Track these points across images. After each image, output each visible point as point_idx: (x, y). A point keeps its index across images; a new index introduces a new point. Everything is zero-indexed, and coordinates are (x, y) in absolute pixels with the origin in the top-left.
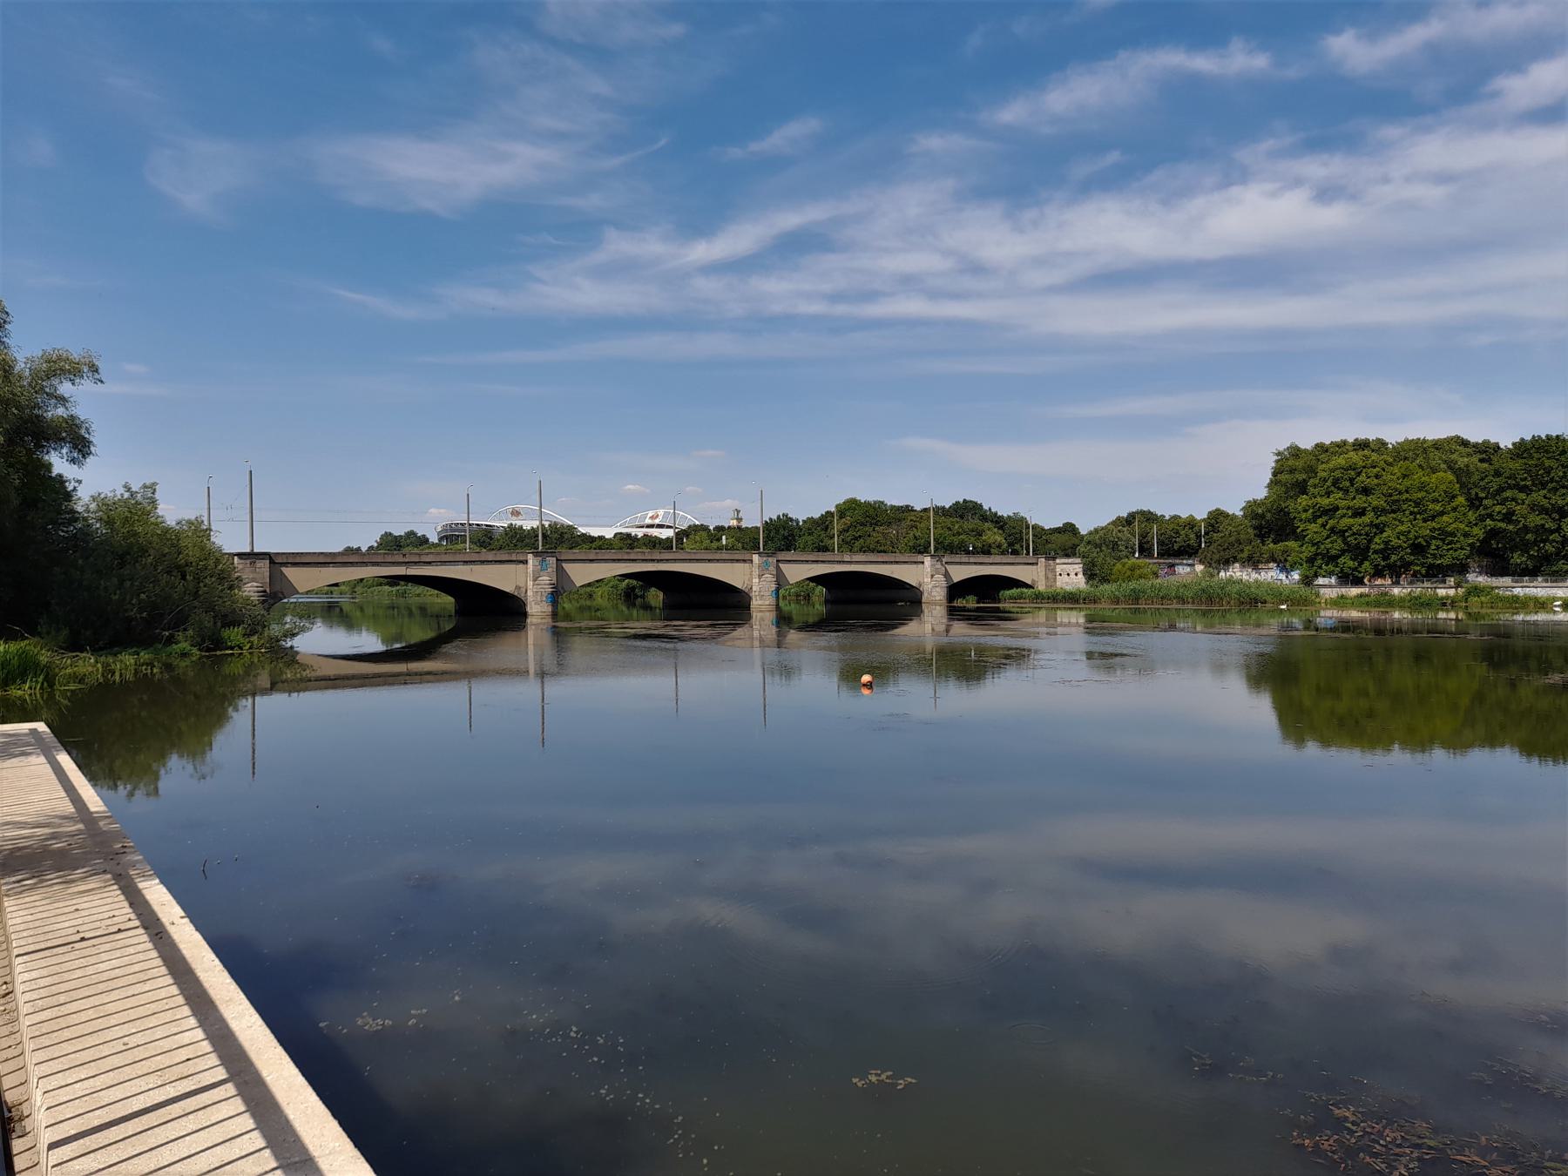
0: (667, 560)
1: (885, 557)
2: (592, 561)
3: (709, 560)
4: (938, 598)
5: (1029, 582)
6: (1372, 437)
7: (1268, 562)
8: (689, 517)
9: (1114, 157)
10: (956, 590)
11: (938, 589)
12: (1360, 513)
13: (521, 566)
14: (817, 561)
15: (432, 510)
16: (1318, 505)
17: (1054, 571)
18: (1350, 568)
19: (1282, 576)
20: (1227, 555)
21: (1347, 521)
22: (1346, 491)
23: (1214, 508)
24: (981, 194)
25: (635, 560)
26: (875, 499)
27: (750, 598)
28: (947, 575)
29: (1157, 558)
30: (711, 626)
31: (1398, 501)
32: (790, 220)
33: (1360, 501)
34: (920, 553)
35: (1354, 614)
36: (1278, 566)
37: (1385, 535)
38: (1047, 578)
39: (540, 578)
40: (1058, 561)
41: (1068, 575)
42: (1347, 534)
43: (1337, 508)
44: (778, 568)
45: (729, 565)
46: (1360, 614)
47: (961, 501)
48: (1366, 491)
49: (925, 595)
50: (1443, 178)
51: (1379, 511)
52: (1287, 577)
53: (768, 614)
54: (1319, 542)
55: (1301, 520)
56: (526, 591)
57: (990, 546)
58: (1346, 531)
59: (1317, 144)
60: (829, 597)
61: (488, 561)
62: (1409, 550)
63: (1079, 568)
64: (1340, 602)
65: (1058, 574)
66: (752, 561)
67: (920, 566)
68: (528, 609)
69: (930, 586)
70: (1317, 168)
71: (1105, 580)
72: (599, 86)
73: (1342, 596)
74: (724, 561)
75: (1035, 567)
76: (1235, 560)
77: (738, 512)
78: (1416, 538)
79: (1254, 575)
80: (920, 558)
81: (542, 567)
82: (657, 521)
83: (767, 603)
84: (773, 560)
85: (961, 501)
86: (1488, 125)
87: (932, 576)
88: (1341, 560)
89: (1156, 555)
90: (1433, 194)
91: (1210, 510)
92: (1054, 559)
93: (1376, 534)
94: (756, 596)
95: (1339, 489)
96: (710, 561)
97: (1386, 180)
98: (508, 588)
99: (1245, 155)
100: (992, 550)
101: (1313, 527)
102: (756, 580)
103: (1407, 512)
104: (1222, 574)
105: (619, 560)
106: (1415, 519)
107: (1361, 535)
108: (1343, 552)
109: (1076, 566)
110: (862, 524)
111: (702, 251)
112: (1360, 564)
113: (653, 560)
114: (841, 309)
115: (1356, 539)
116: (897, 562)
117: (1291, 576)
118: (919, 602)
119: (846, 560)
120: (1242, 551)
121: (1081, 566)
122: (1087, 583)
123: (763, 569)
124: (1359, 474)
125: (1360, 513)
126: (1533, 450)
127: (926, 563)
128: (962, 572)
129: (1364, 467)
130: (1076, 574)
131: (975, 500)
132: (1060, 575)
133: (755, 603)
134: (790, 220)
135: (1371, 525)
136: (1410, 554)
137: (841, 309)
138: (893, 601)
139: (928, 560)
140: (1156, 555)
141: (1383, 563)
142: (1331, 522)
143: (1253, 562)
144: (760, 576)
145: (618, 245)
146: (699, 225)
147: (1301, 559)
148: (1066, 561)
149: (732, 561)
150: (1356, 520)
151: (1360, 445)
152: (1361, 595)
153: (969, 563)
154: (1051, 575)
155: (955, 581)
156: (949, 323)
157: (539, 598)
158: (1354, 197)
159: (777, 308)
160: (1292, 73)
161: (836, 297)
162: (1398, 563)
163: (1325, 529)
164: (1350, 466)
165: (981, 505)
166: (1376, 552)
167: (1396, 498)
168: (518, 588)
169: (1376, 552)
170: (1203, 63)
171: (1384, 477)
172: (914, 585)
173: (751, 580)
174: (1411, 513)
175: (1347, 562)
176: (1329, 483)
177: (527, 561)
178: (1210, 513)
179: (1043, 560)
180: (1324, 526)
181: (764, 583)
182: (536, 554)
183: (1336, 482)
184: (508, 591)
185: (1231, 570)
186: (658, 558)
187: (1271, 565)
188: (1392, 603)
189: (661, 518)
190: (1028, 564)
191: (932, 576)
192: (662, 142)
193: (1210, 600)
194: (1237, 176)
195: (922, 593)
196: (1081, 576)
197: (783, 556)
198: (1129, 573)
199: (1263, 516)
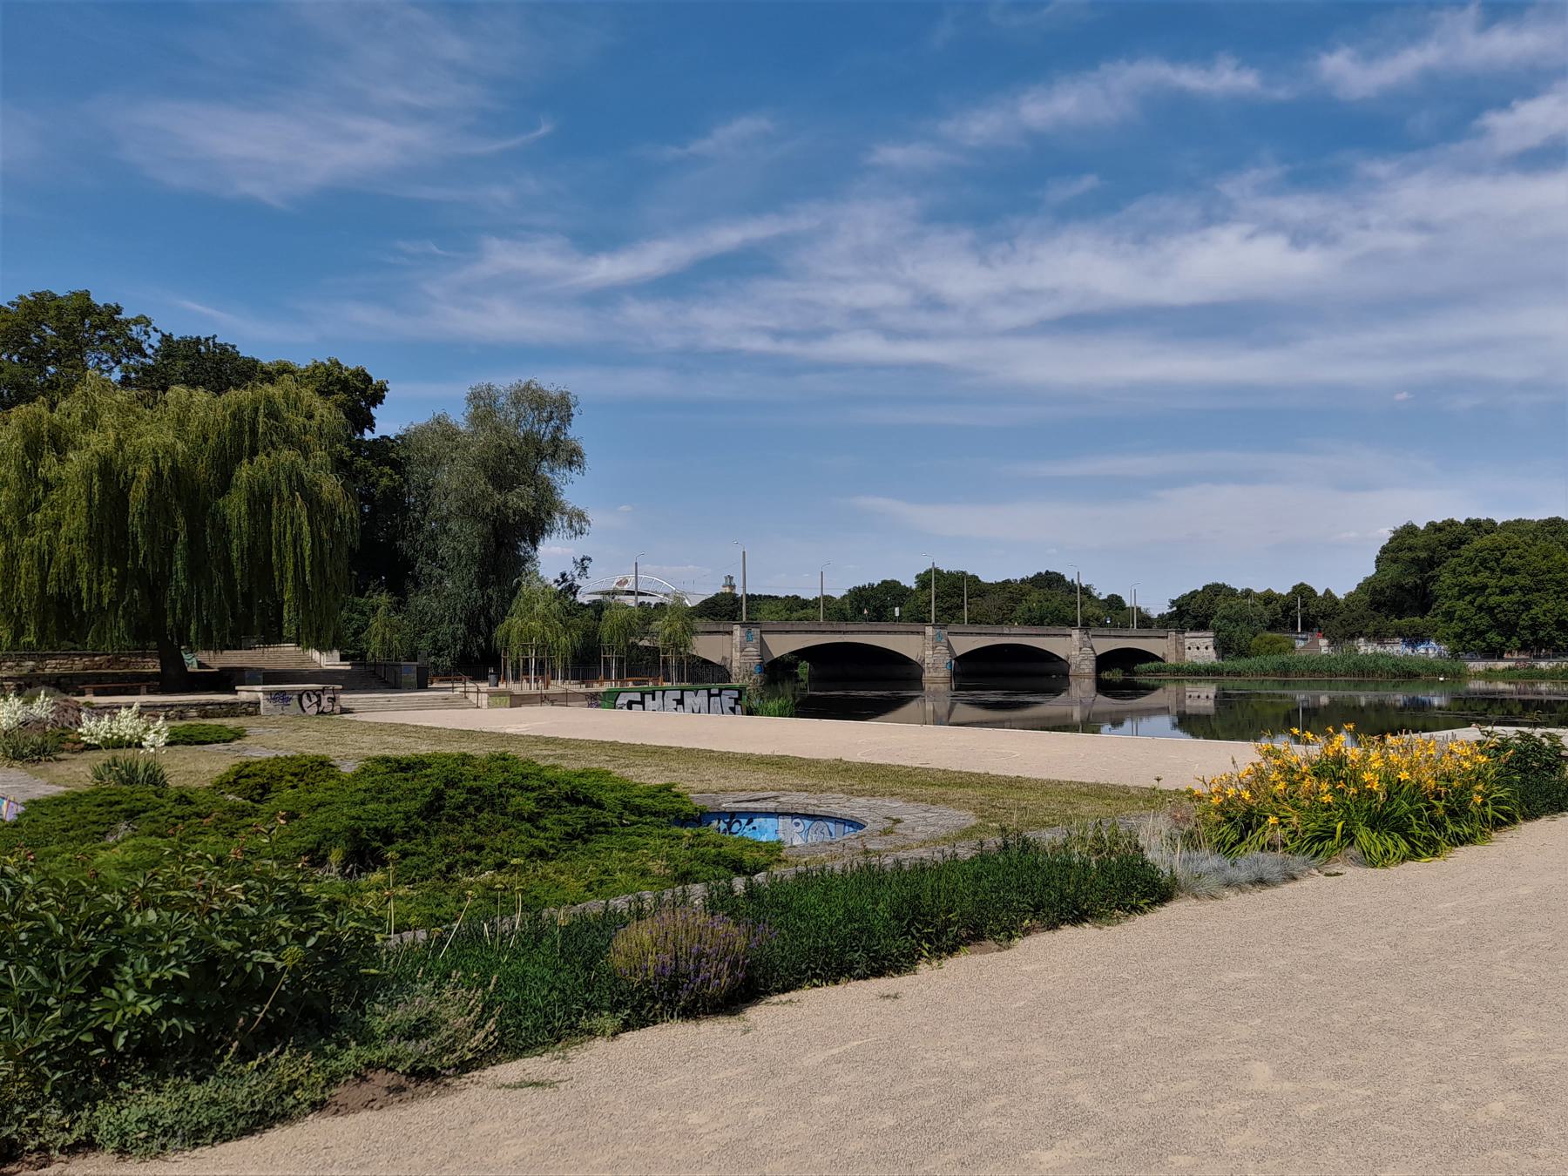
1: (1039, 630)
2: (787, 632)
4: (1087, 671)
6: (1483, 518)
7: (1394, 636)
9: (1089, 182)
10: (1104, 662)
11: (1087, 662)
12: (1505, 591)
13: (727, 636)
17: (1182, 644)
19: (1409, 651)
20: (1352, 629)
21: (1494, 600)
22: (1492, 570)
24: (938, 217)
27: (923, 670)
31: (1543, 581)
32: (727, 237)
33: (1507, 581)
34: (1070, 626)
35: (1501, 686)
36: (1404, 641)
37: (1533, 612)
38: (1177, 651)
40: (1186, 635)
41: (1198, 648)
43: (1485, 587)
45: (719, 637)
46: (1507, 687)
47: (1044, 572)
48: (1512, 571)
49: (1073, 667)
50: (1421, 226)
58: (1495, 608)
59: (1301, 180)
62: (1554, 626)
63: (1209, 642)
64: (1489, 675)
67: (1069, 638)
69: (1078, 659)
70: (1297, 208)
71: (1243, 653)
72: (454, 48)
73: (1490, 670)
75: (1165, 640)
76: (1361, 634)
77: (731, 578)
78: (1560, 615)
79: (1379, 649)
80: (1068, 631)
81: (748, 638)
84: (944, 632)
85: (1044, 572)
86: (1473, 169)
88: (1490, 635)
90: (1410, 241)
95: (1486, 568)
96: (888, 632)
97: (1365, 226)
99: (1230, 188)
100: (1092, 624)
103: (1551, 591)
105: (811, 632)
106: (1558, 598)
107: (1509, 612)
108: (1490, 628)
109: (1207, 640)
110: (949, 595)
111: (607, 269)
112: (1509, 639)
114: (788, 347)
118: (1066, 675)
120: (1367, 626)
122: (1218, 658)
123: (937, 640)
124: (1503, 555)
125: (1505, 591)
127: (1074, 636)
128: (1105, 645)
129: (1508, 548)
130: (1207, 648)
131: (1058, 572)
133: (927, 675)
134: (727, 237)
135: (1519, 602)
136: (1557, 630)
137: (788, 347)
138: (1048, 675)
139: (738, 631)
142: (1480, 600)
143: (1379, 636)
144: (934, 648)
145: (502, 257)
146: (594, 241)
149: (907, 632)
152: (1510, 669)
153: (1110, 636)
154: (1180, 648)
155: (776, 655)
160: (1281, 94)
161: (779, 335)
162: (1546, 639)
165: (1063, 576)
167: (1541, 578)
168: (724, 659)
169: (1524, 628)
170: (1189, 78)
173: (923, 651)
174: (1555, 592)
175: (1494, 638)
176: (1476, 563)
178: (1294, 587)
180: (1472, 603)
182: (743, 625)
183: (1483, 562)
187: (1397, 640)
188: (1543, 676)
190: (1159, 637)
192: (545, 129)
193: (1362, 673)
194: (1214, 216)
195: (1069, 666)
196: (1211, 649)
197: (952, 628)
198: (1268, 647)
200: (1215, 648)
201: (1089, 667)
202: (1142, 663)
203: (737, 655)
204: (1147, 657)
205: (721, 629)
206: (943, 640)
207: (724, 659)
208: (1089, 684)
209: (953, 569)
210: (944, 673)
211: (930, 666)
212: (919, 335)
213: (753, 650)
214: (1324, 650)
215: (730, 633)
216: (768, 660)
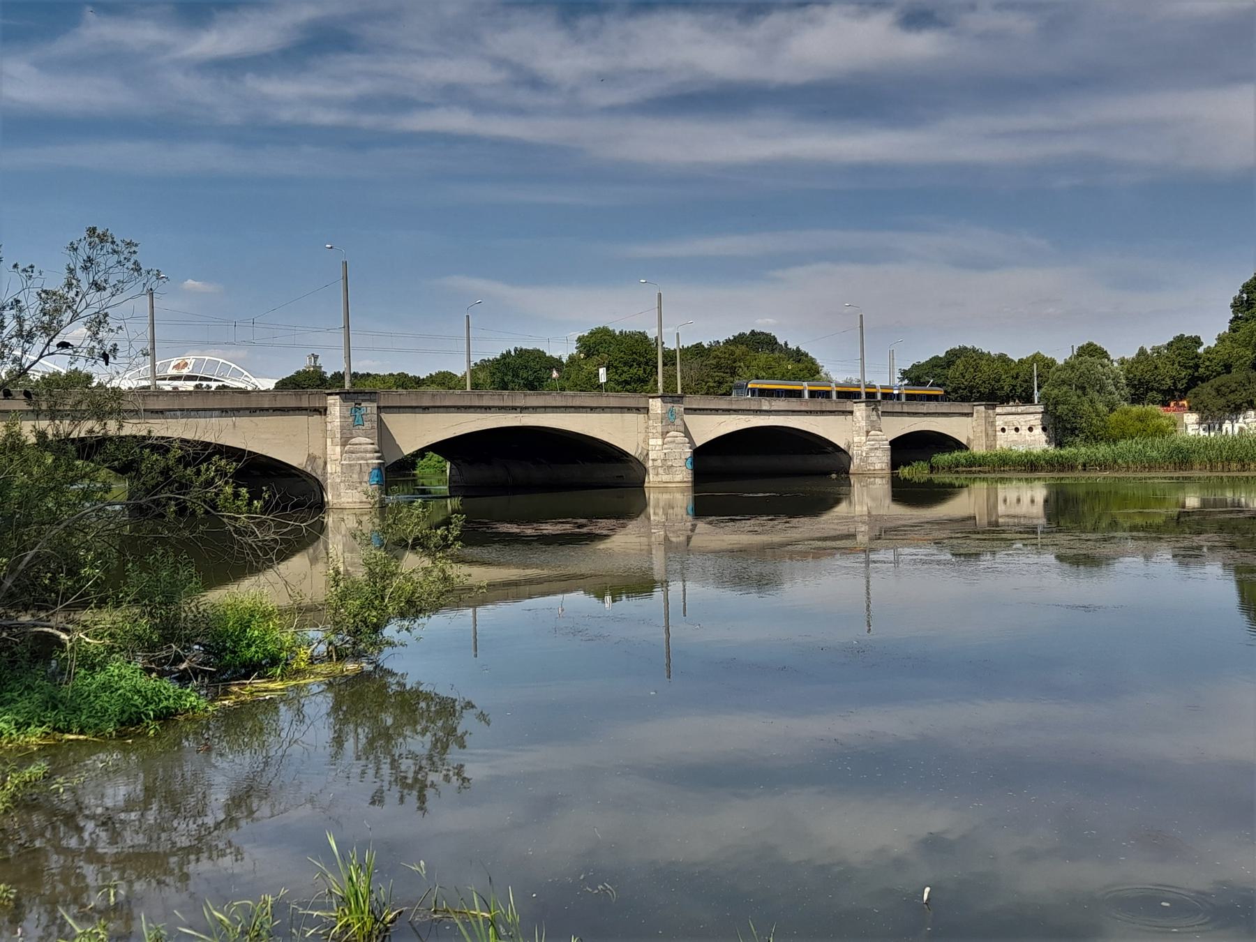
0: (533, 408)
2: (426, 409)
4: (878, 466)
11: (879, 453)
15: (190, 282)
17: (993, 424)
20: (1236, 398)
27: (645, 470)
28: (384, 436)
38: (987, 435)
39: (353, 441)
41: (1017, 430)
45: (302, 419)
47: (748, 333)
56: (325, 463)
61: (262, 410)
63: (1036, 420)
65: (998, 428)
68: (329, 497)
69: (864, 448)
74: (612, 409)
77: (316, 357)
82: (185, 372)
83: (679, 478)
84: (679, 408)
87: (868, 432)
89: (1036, 402)
91: (1081, 345)
94: (655, 467)
98: (294, 458)
104: (1227, 425)
109: (1031, 417)
114: (368, 121)
119: (764, 408)
121: (1040, 416)
122: (1048, 442)
123: (668, 420)
130: (1030, 429)
132: (1003, 430)
133: (652, 479)
140: (1036, 402)
144: (664, 434)
153: (901, 414)
156: (498, 143)
157: (355, 476)
158: (942, 24)
159: (286, 115)
161: (364, 104)
168: (312, 459)
173: (646, 441)
177: (326, 410)
181: (672, 446)
184: (295, 464)
185: (1241, 420)
189: (191, 367)
191: (868, 432)
195: (850, 459)
196: (1038, 431)
200: (1044, 429)
201: (881, 460)
202: (943, 452)
203: (334, 451)
204: (946, 443)
205: (305, 404)
206: (678, 422)
207: (312, 459)
208: (882, 486)
209: (627, 330)
210: (683, 474)
211: (659, 463)
212: (518, 111)
213: (364, 442)
214: (1191, 431)
215: (322, 411)
216: (391, 460)
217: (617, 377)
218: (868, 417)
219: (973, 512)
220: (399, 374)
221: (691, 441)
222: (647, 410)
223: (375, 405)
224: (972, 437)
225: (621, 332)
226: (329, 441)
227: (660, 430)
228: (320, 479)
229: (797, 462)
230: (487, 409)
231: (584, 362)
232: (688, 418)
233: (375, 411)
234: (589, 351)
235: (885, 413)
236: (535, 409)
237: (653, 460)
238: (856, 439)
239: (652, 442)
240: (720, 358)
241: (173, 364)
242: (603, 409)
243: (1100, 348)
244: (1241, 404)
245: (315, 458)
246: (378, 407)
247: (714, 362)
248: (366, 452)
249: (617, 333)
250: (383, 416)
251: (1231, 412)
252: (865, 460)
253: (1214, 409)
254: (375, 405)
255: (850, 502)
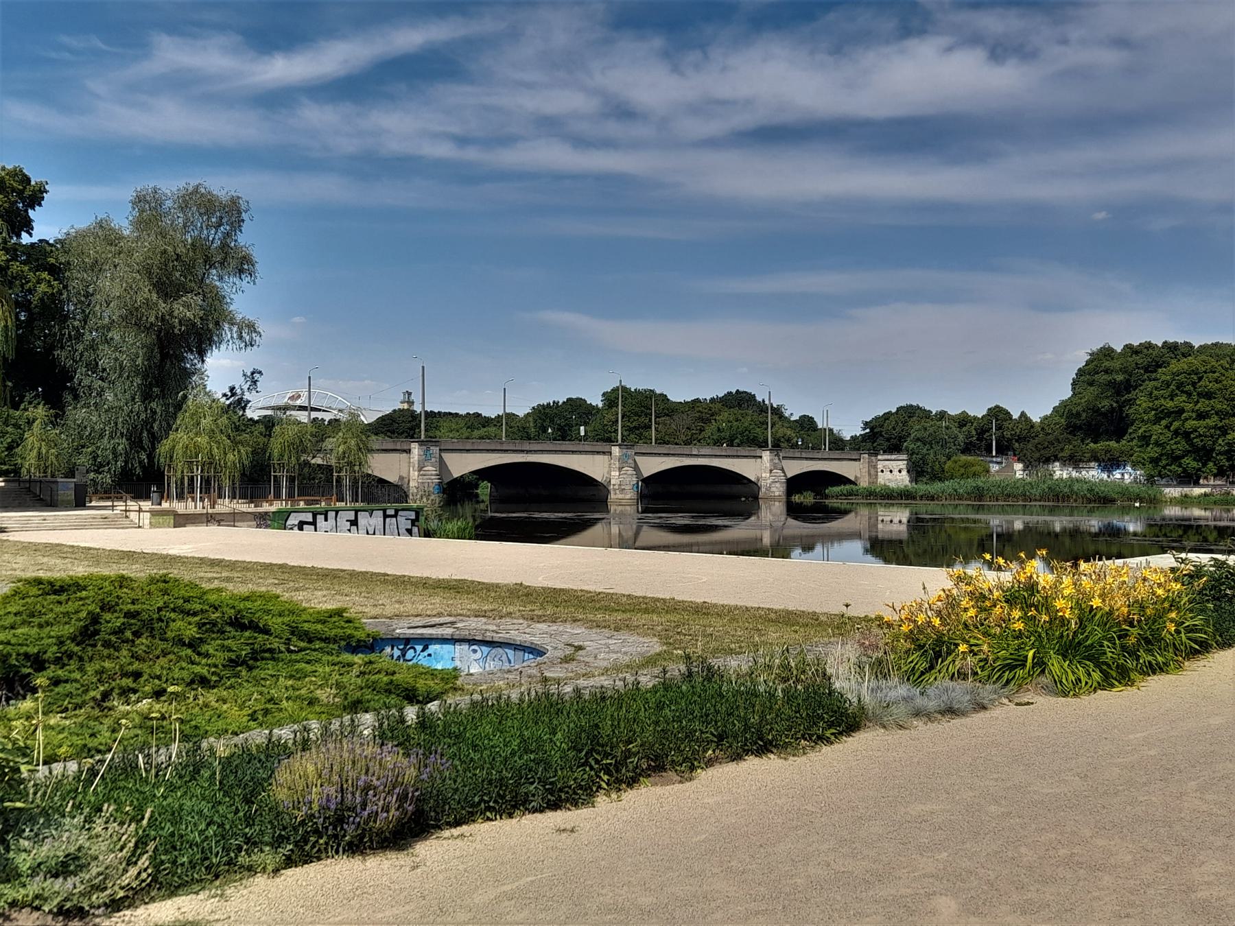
2: (468, 451)
3: (573, 452)
4: (777, 494)
5: (853, 478)
6: (1181, 340)
7: (1090, 461)
8: (340, 398)
10: (795, 484)
12: (1201, 416)
13: (405, 455)
14: (668, 455)
16: (1163, 407)
17: (875, 467)
18: (1194, 468)
19: (1105, 476)
20: (1047, 453)
21: (1191, 423)
22: (1189, 394)
23: (993, 405)
25: (507, 450)
26: (645, 388)
27: (609, 492)
28: (442, 465)
29: (996, 456)
30: (693, 517)
33: (1203, 405)
34: (760, 447)
35: (1197, 512)
36: (1099, 465)
38: (870, 474)
40: (879, 457)
41: (891, 471)
42: (1192, 436)
43: (1182, 411)
44: (441, 461)
47: (734, 391)
48: (1209, 395)
49: (763, 490)
51: (1222, 414)
52: (1109, 477)
53: (628, 508)
54: (1164, 443)
55: (1143, 421)
57: (779, 440)
58: (1192, 432)
60: (495, 494)
64: (1185, 501)
65: (879, 470)
66: (611, 453)
67: (759, 460)
69: (769, 481)
71: (936, 477)
74: (586, 452)
77: (410, 394)
79: (1074, 474)
80: (758, 452)
82: (298, 403)
83: (628, 496)
84: (631, 452)
90: (1110, 58)
91: (990, 407)
92: (876, 455)
93: (1219, 436)
94: (615, 490)
95: (1183, 392)
98: (392, 478)
101: (1157, 428)
102: (615, 473)
105: (493, 451)
109: (900, 463)
112: (1205, 465)
113: (522, 451)
114: (472, 154)
115: (1202, 441)
116: (738, 457)
117: (1113, 475)
119: (694, 453)
121: (905, 462)
122: (911, 481)
123: (623, 461)
124: (1200, 379)
126: (1215, 350)
128: (796, 467)
129: (1205, 372)
130: (900, 471)
132: (882, 471)
133: (613, 496)
135: (1215, 427)
137: (472, 154)
138: (736, 497)
141: (1227, 464)
142: (1176, 424)
143: (1074, 461)
144: (620, 469)
147: (1144, 459)
148: (886, 457)
149: (593, 453)
150: (1201, 422)
151: (1170, 348)
152: (1205, 495)
154: (873, 472)
161: (462, 141)
163: (1169, 430)
164: (1193, 371)
166: (1220, 453)
168: (401, 478)
169: (1220, 453)
171: (1225, 382)
172: (753, 480)
173: (609, 473)
175: (1190, 463)
177: (410, 450)
178: (989, 409)
179: (866, 456)
180: (1167, 427)
181: (625, 476)
182: (421, 443)
183: (1180, 386)
186: (528, 448)
187: (1092, 464)
191: (771, 471)
195: (759, 488)
196: (904, 473)
198: (962, 470)
199: (1078, 415)
200: (908, 472)
201: (779, 490)
203: (414, 474)
206: (630, 461)
207: (401, 478)
208: (779, 507)
210: (630, 495)
211: (617, 487)
212: (608, 144)
213: (431, 469)
214: (1019, 475)
216: (446, 480)
217: (629, 424)
218: (771, 460)
219: (858, 528)
220: (474, 414)
221: (785, 476)
222: (610, 453)
223: (438, 448)
224: (859, 475)
225: (635, 390)
226: (411, 469)
227: (617, 466)
228: (406, 490)
229: (726, 489)
230: (506, 451)
231: (606, 412)
232: (638, 458)
233: (438, 451)
234: (610, 403)
235: (784, 458)
236: (536, 452)
237: (614, 485)
238: (764, 475)
239: (613, 473)
240: (702, 413)
241: (289, 395)
242: (580, 452)
243: (1004, 410)
244: (1049, 457)
245: (403, 478)
246: (440, 450)
247: (697, 415)
248: (432, 475)
249: (633, 390)
250: (443, 454)
251: (1044, 463)
252: (769, 489)
253: (1032, 460)
254: (438, 448)
255: (758, 517)
